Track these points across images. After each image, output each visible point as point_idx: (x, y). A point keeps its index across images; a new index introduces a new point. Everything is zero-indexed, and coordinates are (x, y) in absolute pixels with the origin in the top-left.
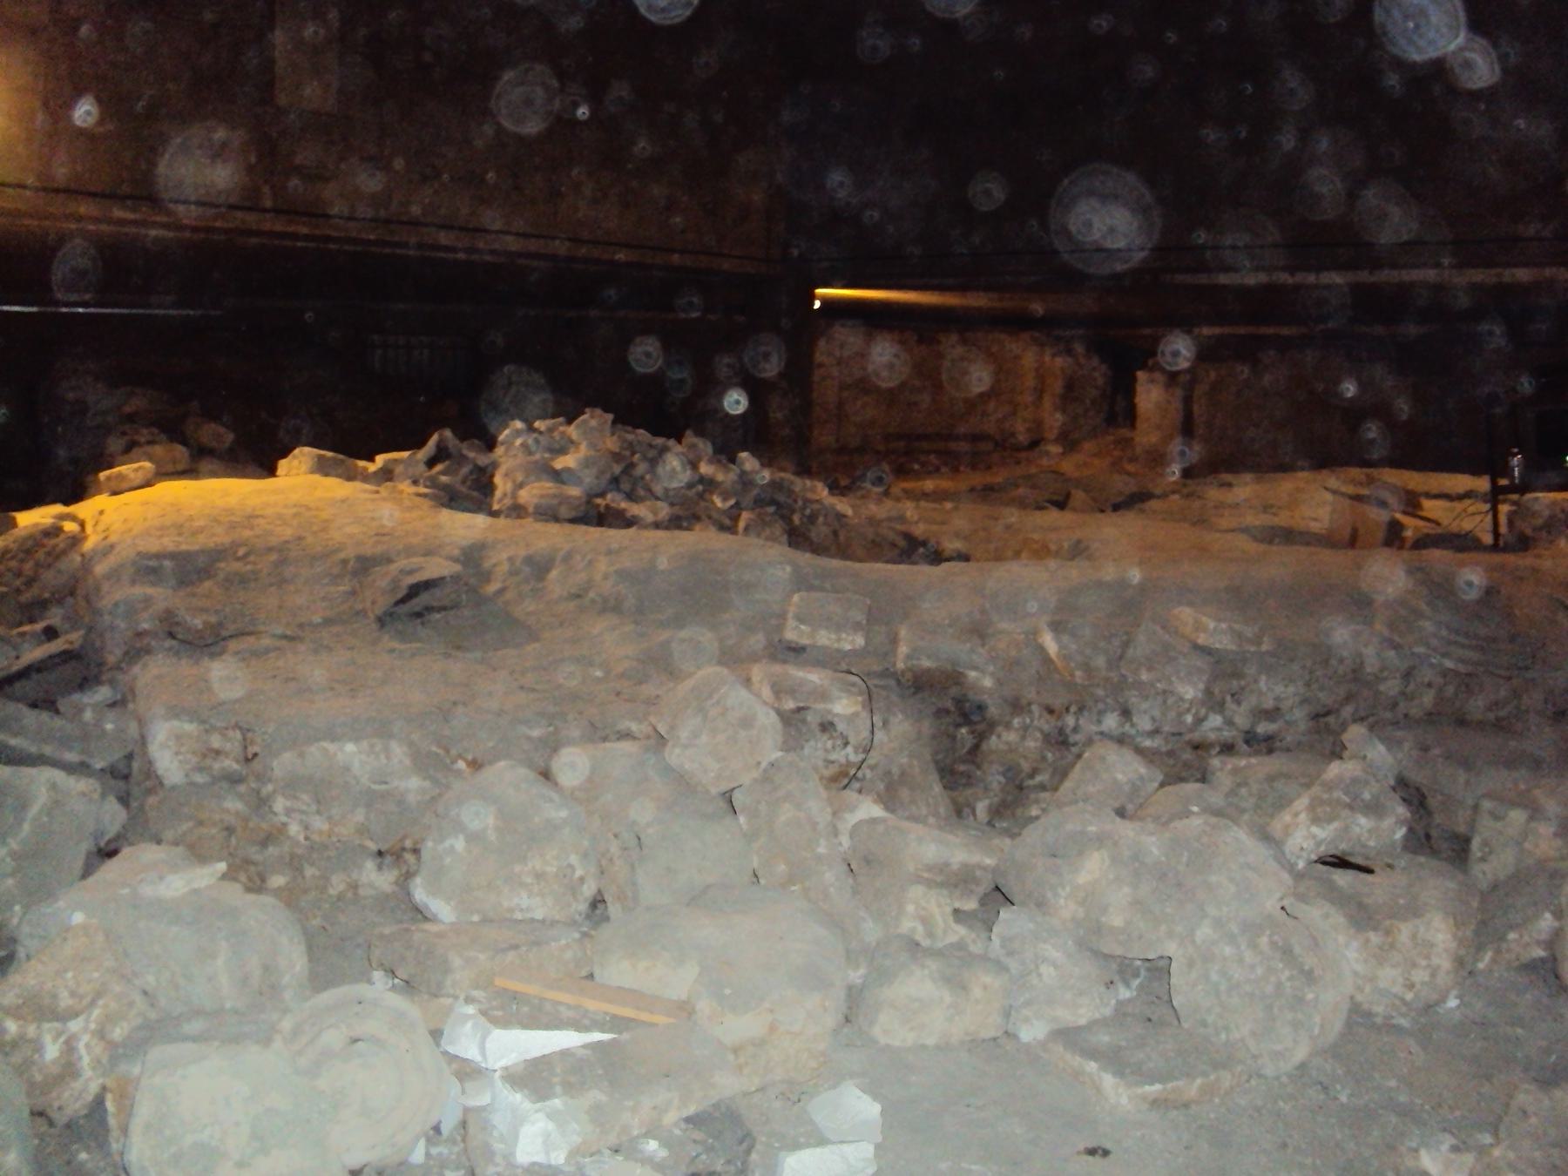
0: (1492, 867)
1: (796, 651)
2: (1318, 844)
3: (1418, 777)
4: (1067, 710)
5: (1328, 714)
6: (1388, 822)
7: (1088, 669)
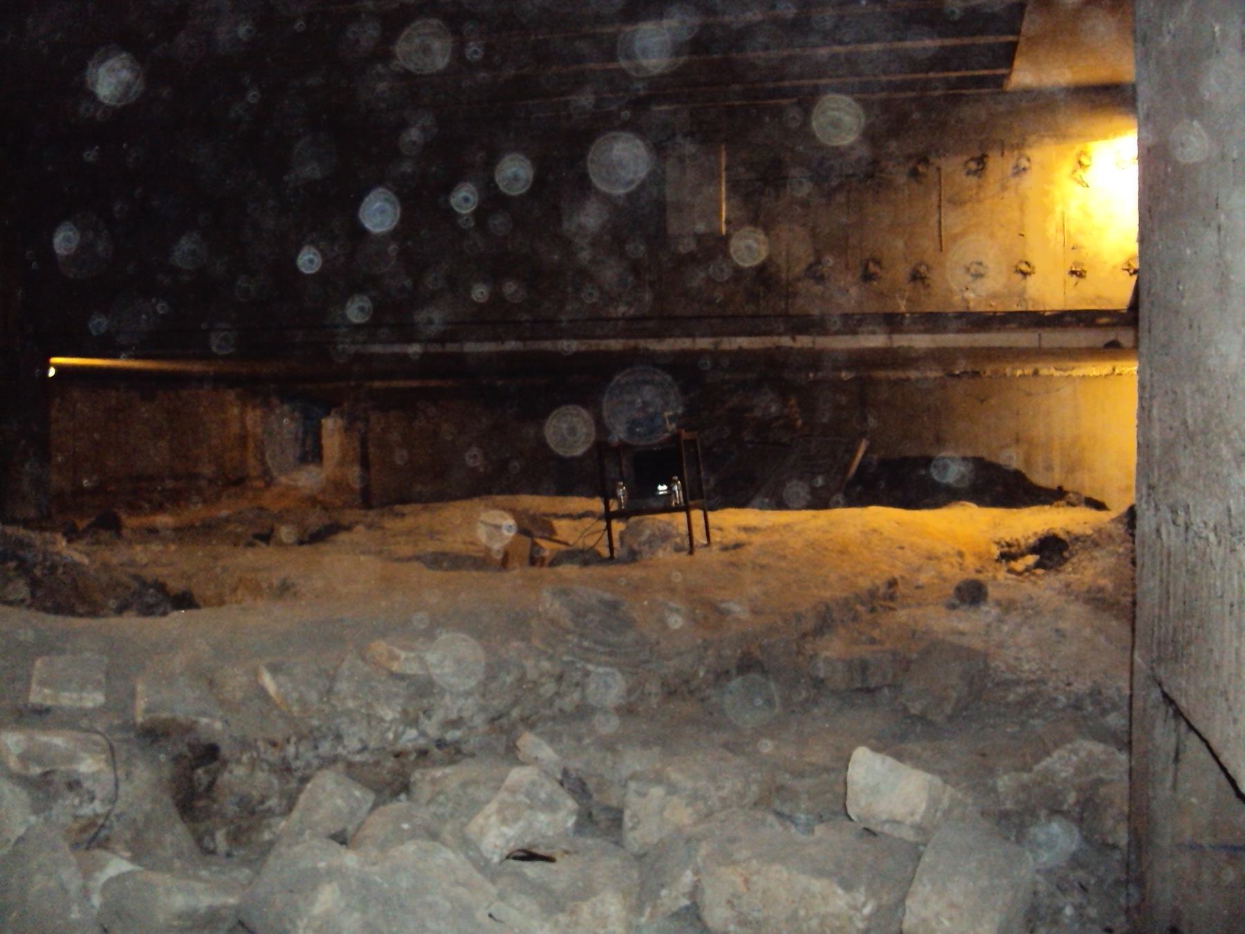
0: (640, 835)
1: (42, 712)
2: (508, 841)
3: (575, 765)
4: (288, 741)
5: (501, 716)
6: (561, 814)
7: (302, 702)
